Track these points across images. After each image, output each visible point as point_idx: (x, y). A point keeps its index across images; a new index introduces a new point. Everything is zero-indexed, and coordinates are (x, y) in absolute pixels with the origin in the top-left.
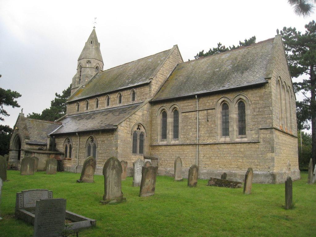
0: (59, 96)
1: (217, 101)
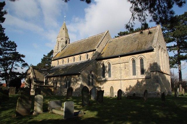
0: (45, 56)
1: (129, 58)
